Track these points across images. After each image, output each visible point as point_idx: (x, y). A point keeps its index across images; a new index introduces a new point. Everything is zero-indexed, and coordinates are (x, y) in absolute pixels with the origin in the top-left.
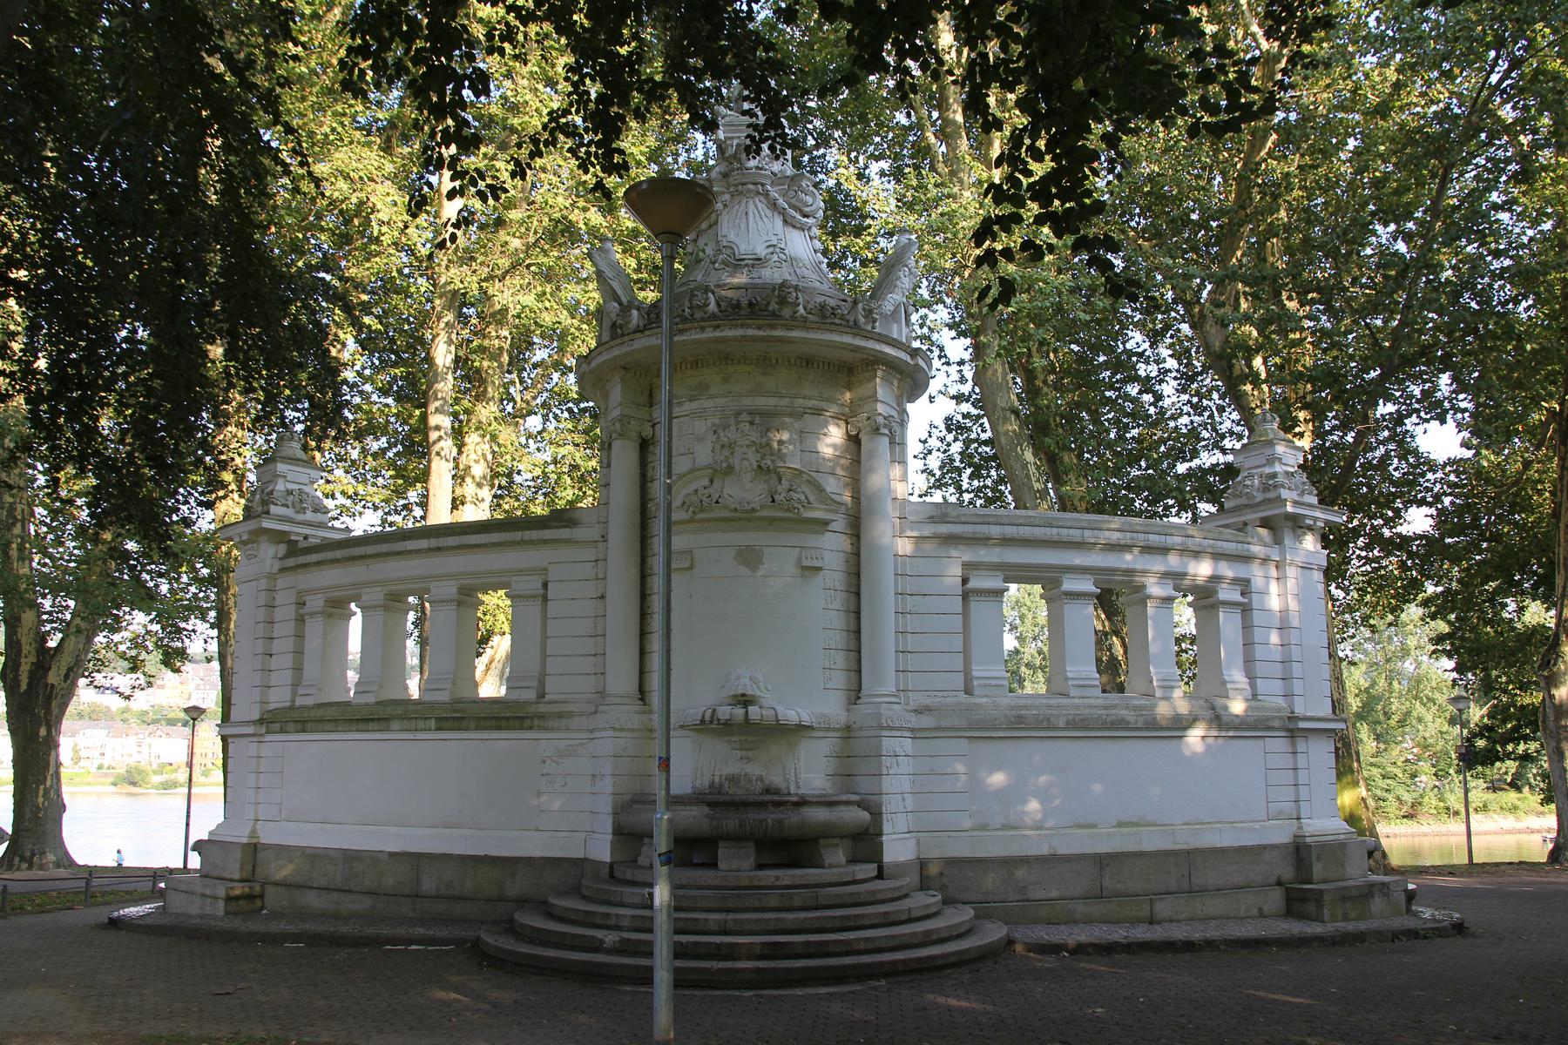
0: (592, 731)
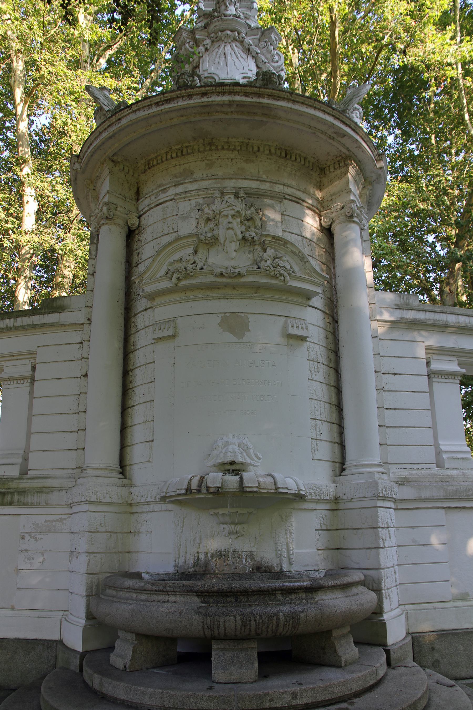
0: (71, 505)
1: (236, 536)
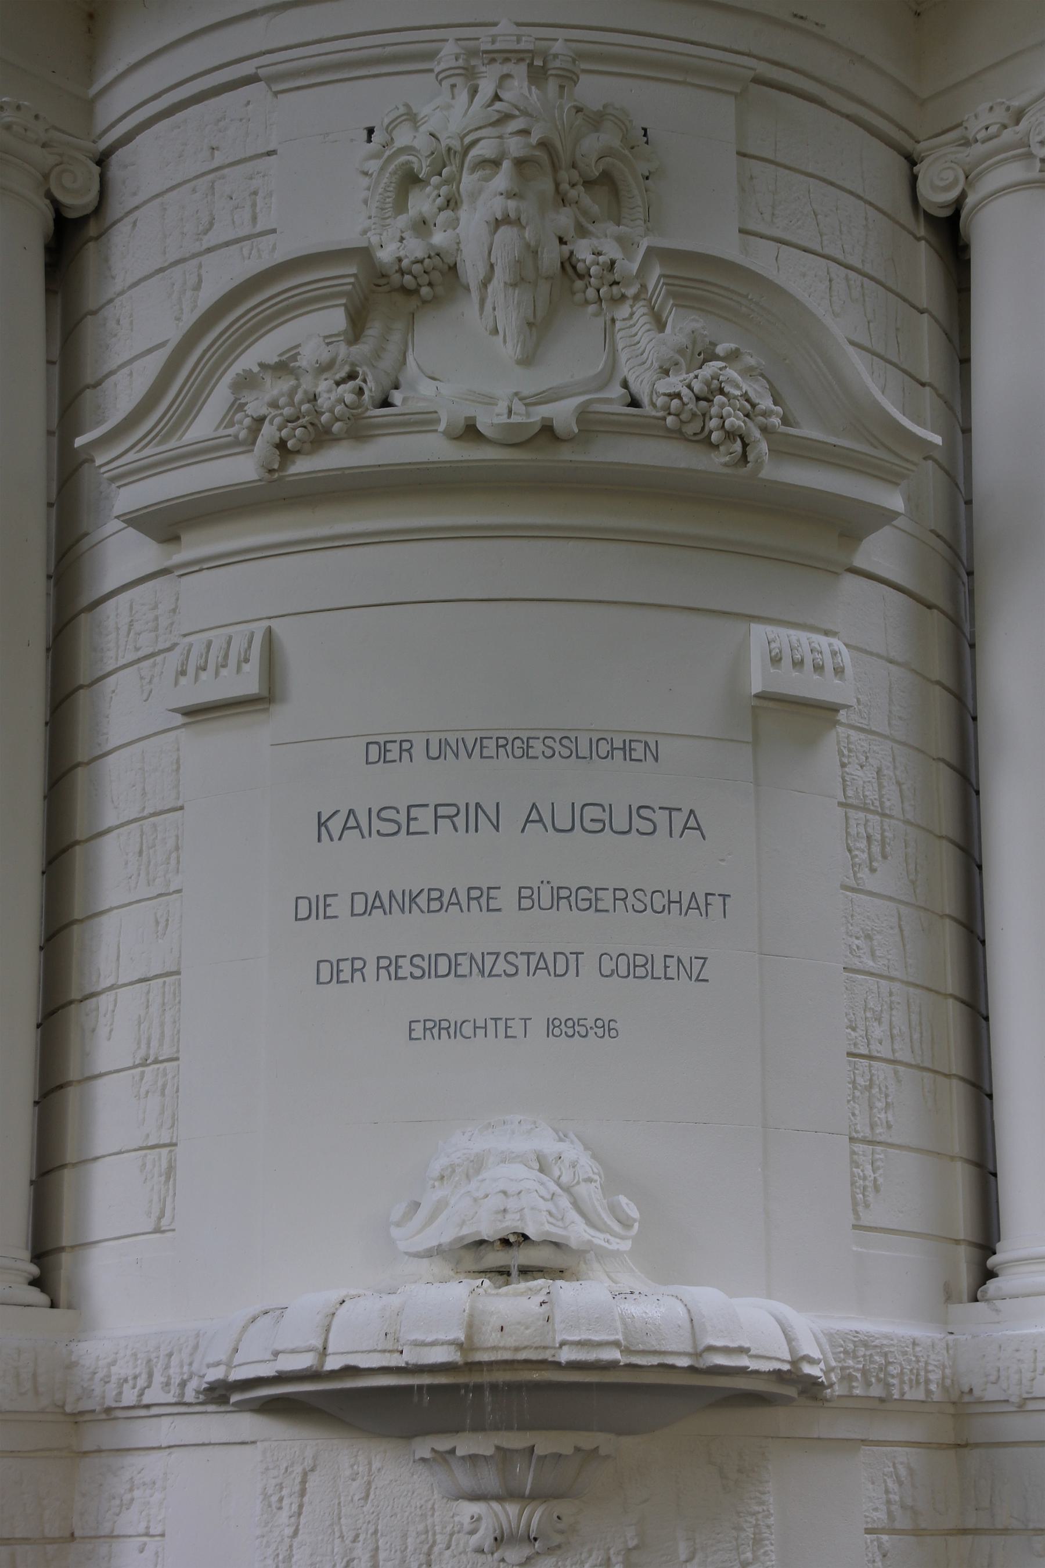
1: (527, 1551)
